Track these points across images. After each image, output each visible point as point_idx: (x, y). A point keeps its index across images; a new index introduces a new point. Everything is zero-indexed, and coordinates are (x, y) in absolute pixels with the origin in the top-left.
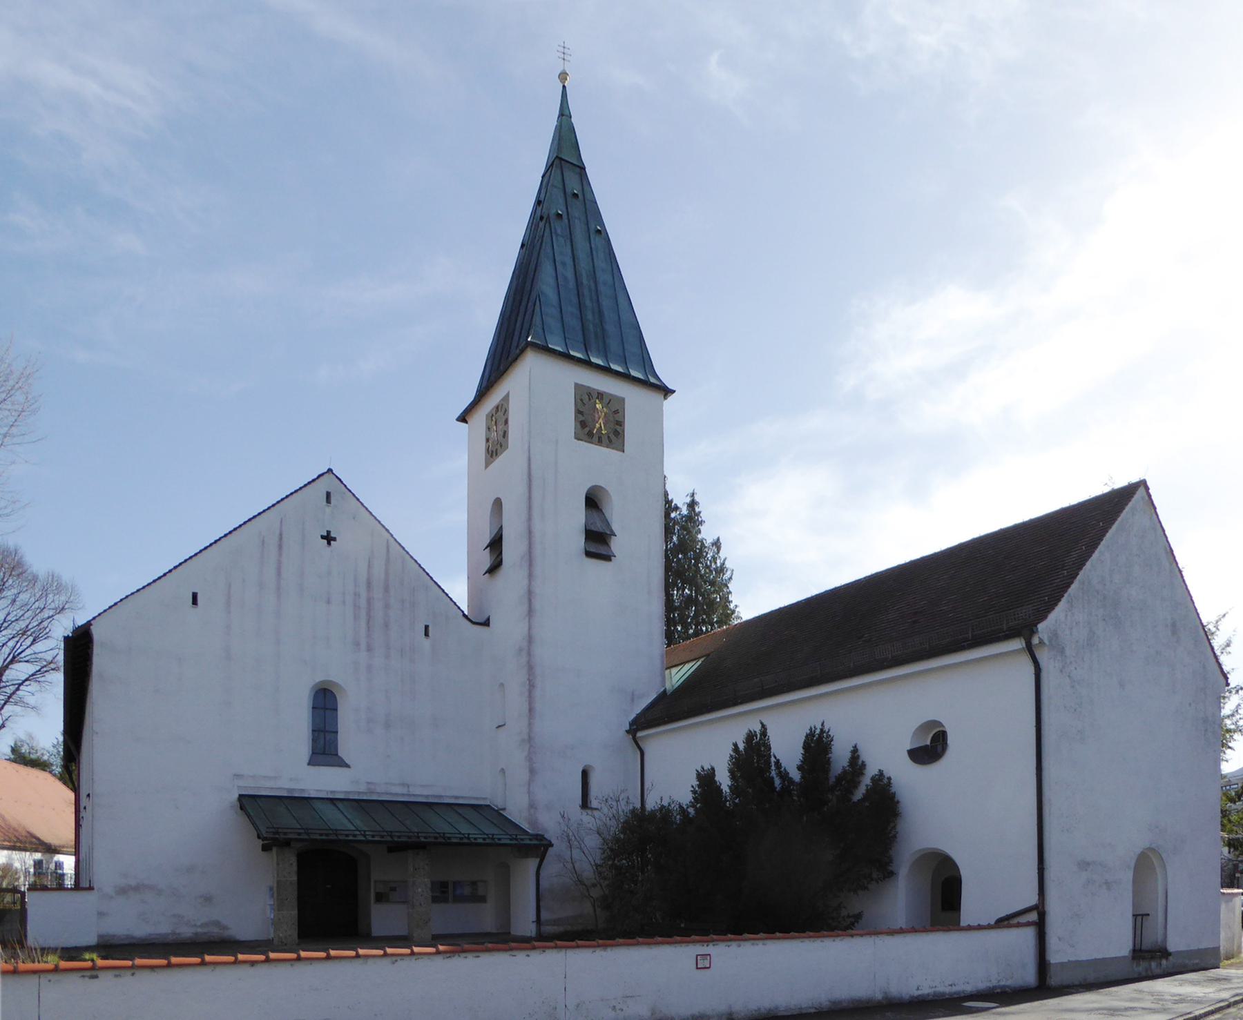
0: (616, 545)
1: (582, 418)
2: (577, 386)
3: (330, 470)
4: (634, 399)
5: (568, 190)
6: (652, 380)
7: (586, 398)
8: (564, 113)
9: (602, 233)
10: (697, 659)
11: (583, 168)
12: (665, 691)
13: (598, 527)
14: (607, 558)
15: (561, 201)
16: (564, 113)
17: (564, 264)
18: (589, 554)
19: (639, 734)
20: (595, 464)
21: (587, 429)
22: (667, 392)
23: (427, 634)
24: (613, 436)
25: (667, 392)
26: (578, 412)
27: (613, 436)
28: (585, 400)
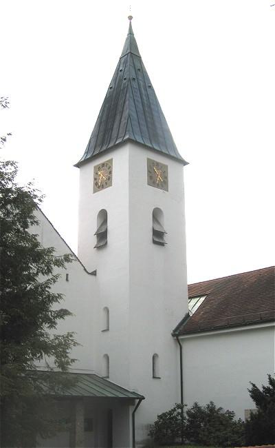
0: (166, 238)
1: (151, 175)
2: (148, 159)
3: (154, 377)
4: (172, 167)
5: (137, 68)
6: (172, 154)
7: (151, 165)
8: (131, 33)
9: (150, 87)
10: (200, 296)
11: (140, 57)
12: (188, 315)
13: (158, 228)
14: (162, 244)
15: (134, 72)
16: (131, 33)
17: (138, 101)
18: (155, 242)
19: (180, 337)
20: (155, 197)
21: (152, 181)
22: (185, 163)
23: (67, 280)
24: (163, 185)
25: (185, 163)
26: (149, 172)
27: (163, 185)
28: (151, 165)
